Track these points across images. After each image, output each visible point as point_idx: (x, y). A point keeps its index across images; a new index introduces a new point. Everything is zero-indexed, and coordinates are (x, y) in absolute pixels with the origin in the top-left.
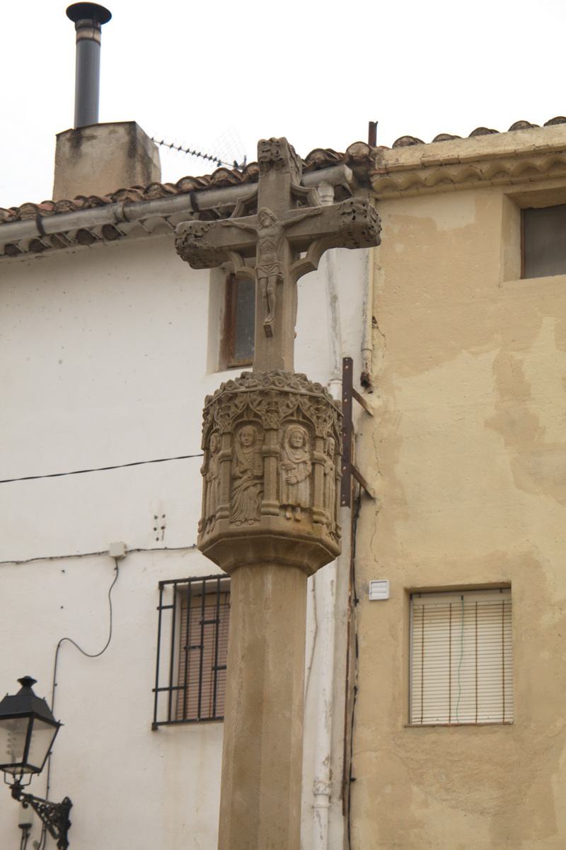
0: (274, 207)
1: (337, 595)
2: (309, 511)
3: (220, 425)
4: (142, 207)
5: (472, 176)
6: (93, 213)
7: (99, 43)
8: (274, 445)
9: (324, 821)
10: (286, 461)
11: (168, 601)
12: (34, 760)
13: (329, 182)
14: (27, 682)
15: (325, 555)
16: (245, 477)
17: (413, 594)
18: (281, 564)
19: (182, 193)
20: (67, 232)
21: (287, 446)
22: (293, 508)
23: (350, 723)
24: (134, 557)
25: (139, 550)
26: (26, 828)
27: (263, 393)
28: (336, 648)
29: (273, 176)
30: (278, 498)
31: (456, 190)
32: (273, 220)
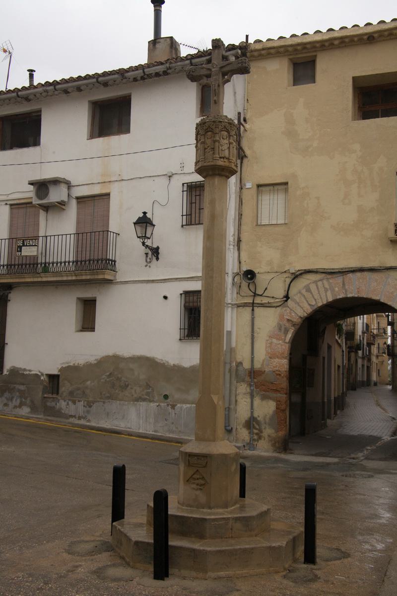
0: (217, 61)
1: (236, 187)
2: (228, 159)
3: (201, 132)
4: (176, 64)
5: (278, 52)
6: (160, 67)
7: (161, 11)
8: (217, 138)
9: (232, 252)
10: (221, 143)
11: (185, 189)
12: (148, 235)
13: (233, 55)
14: (145, 213)
15: (233, 172)
16: (209, 148)
17: (259, 186)
18: (220, 175)
19: (187, 59)
20: (152, 73)
21: (221, 138)
22: (223, 158)
23: (240, 225)
24: (175, 176)
25: (176, 174)
26: (147, 254)
27: (214, 122)
28: (236, 203)
29: (216, 51)
30: (219, 155)
31: (273, 57)
32: (217, 66)
